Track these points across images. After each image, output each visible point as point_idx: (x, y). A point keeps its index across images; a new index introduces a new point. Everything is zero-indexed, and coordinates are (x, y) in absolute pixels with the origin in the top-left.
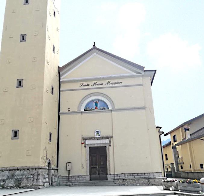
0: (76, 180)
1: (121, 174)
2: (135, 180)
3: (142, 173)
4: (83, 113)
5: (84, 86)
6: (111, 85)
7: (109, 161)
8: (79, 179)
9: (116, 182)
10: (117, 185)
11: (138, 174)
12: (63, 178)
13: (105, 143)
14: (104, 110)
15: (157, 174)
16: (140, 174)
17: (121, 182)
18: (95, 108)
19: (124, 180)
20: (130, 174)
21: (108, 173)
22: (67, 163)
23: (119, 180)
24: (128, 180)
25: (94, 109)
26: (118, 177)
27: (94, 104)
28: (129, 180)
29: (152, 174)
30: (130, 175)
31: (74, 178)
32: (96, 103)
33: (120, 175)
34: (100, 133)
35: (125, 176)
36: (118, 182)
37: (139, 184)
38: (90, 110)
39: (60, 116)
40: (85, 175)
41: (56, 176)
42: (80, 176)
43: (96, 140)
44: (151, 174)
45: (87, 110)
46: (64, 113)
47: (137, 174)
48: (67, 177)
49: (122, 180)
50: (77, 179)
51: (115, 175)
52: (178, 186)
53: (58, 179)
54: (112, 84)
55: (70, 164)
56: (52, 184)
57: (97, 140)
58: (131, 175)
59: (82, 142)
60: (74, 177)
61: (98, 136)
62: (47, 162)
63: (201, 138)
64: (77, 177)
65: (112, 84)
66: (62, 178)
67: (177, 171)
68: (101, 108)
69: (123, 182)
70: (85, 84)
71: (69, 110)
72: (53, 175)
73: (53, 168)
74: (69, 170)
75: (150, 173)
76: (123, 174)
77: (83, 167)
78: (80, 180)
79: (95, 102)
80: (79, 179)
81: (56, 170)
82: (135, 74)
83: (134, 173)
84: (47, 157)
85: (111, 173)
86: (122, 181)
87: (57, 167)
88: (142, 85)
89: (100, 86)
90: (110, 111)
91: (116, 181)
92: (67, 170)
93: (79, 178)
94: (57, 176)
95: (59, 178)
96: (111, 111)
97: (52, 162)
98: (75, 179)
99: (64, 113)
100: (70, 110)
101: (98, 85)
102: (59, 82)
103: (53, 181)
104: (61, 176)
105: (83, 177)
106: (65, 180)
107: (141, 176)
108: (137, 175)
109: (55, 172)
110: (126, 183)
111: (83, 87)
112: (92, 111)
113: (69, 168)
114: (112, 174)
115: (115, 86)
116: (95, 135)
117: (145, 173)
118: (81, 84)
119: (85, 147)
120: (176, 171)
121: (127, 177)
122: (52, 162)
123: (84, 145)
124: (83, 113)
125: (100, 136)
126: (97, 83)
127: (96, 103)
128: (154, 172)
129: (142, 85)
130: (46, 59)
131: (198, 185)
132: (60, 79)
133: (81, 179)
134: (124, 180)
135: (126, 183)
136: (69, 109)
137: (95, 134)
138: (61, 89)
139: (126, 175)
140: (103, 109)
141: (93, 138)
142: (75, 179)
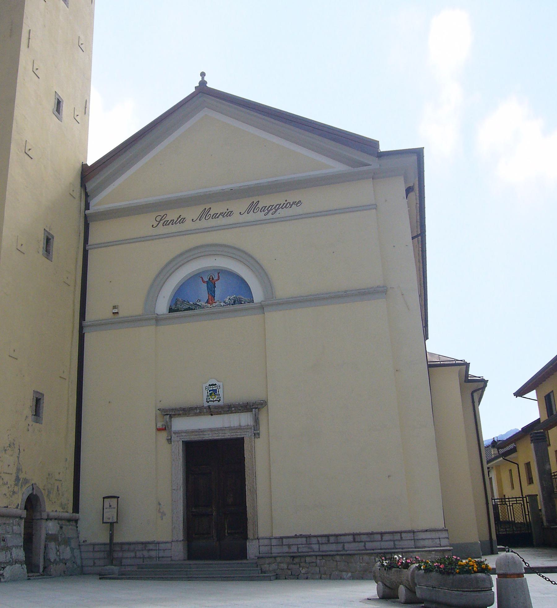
0: (135, 557)
1: (296, 537)
2: (338, 558)
3: (372, 534)
4: (165, 319)
5: (166, 224)
6: (260, 216)
7: (254, 492)
8: (146, 554)
9: (266, 567)
10: (269, 579)
11: (358, 538)
12: (94, 551)
13: (240, 428)
14: (237, 306)
15: (428, 535)
16: (364, 538)
17: (284, 566)
18: (208, 302)
19: (296, 560)
20: (328, 536)
21: (250, 535)
22: (104, 498)
23: (279, 559)
24: (308, 559)
25: (203, 303)
26: (286, 549)
27: (204, 286)
28: (313, 559)
29: (409, 536)
30: (328, 542)
31: (129, 550)
32: (211, 285)
33: (292, 541)
34: (221, 392)
35: (309, 544)
36: (274, 566)
37: (350, 574)
38: (189, 309)
39: (87, 337)
40: (169, 540)
41: (67, 542)
42: (149, 543)
43: (210, 416)
44: (404, 535)
45: (177, 310)
46: (102, 325)
47: (354, 535)
48: (108, 548)
49: (288, 560)
50: (139, 554)
51: (274, 542)
52: (415, 585)
53: (77, 552)
54: (263, 209)
55: (114, 502)
56: (45, 568)
57: (212, 415)
58: (332, 539)
59: (160, 425)
60: (132, 547)
61: (216, 403)
62: (20, 494)
63: (523, 396)
64: (140, 547)
65: (263, 209)
66: (91, 548)
67: (548, 521)
68: (227, 300)
69: (291, 566)
70: (169, 218)
71: (116, 311)
72: (51, 538)
73: (52, 514)
74: (112, 524)
75: (401, 533)
76: (301, 536)
77: (163, 514)
78: (150, 557)
79: (206, 279)
80: (146, 554)
81: (69, 520)
82: (338, 167)
83: (343, 532)
84: (22, 476)
85: (261, 535)
86: (288, 564)
87: (76, 508)
88: (375, 207)
89: (222, 221)
90: (254, 308)
91: (267, 561)
92: (103, 523)
93: (149, 550)
94: (73, 544)
95: (83, 548)
96: (262, 307)
97: (49, 492)
98: (132, 554)
99: (102, 325)
100: (117, 313)
101: (215, 216)
102: (86, 217)
103: (49, 560)
104: (88, 542)
105: (162, 546)
106: (101, 555)
107: (369, 545)
108: (354, 541)
109: (61, 528)
110: (303, 571)
111: (162, 229)
112: (197, 312)
113: (110, 515)
114: (263, 538)
115: (274, 216)
116: (205, 397)
117: (382, 534)
118: (158, 219)
119: (170, 441)
120: (545, 524)
121: (316, 547)
122: (49, 492)
123: (164, 435)
124: (165, 319)
125: (221, 403)
126: (212, 212)
127: (211, 285)
128: (415, 528)
129: (375, 207)
130: (15, 136)
131: (476, 578)
132: (87, 207)
133: (153, 554)
134: (293, 557)
135: (303, 571)
136: (115, 307)
137: (205, 393)
138: (91, 241)
139: (314, 540)
140: (234, 303)
141: (196, 408)
142: (132, 554)
